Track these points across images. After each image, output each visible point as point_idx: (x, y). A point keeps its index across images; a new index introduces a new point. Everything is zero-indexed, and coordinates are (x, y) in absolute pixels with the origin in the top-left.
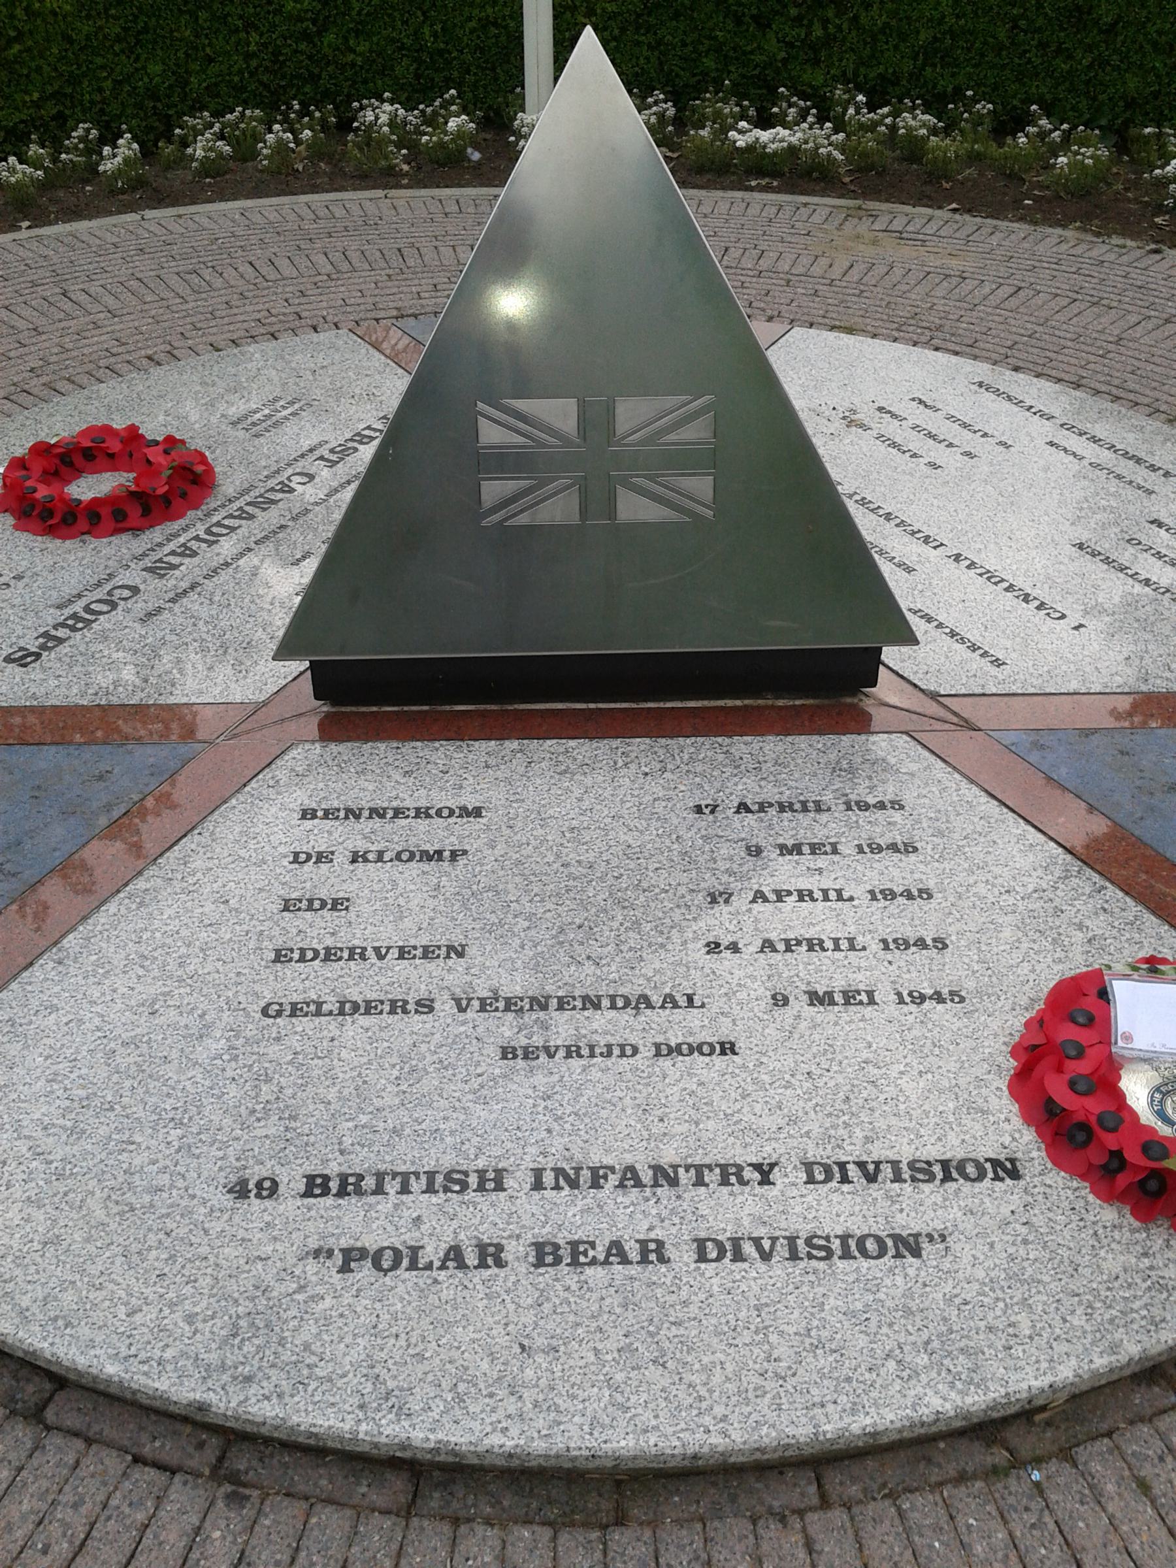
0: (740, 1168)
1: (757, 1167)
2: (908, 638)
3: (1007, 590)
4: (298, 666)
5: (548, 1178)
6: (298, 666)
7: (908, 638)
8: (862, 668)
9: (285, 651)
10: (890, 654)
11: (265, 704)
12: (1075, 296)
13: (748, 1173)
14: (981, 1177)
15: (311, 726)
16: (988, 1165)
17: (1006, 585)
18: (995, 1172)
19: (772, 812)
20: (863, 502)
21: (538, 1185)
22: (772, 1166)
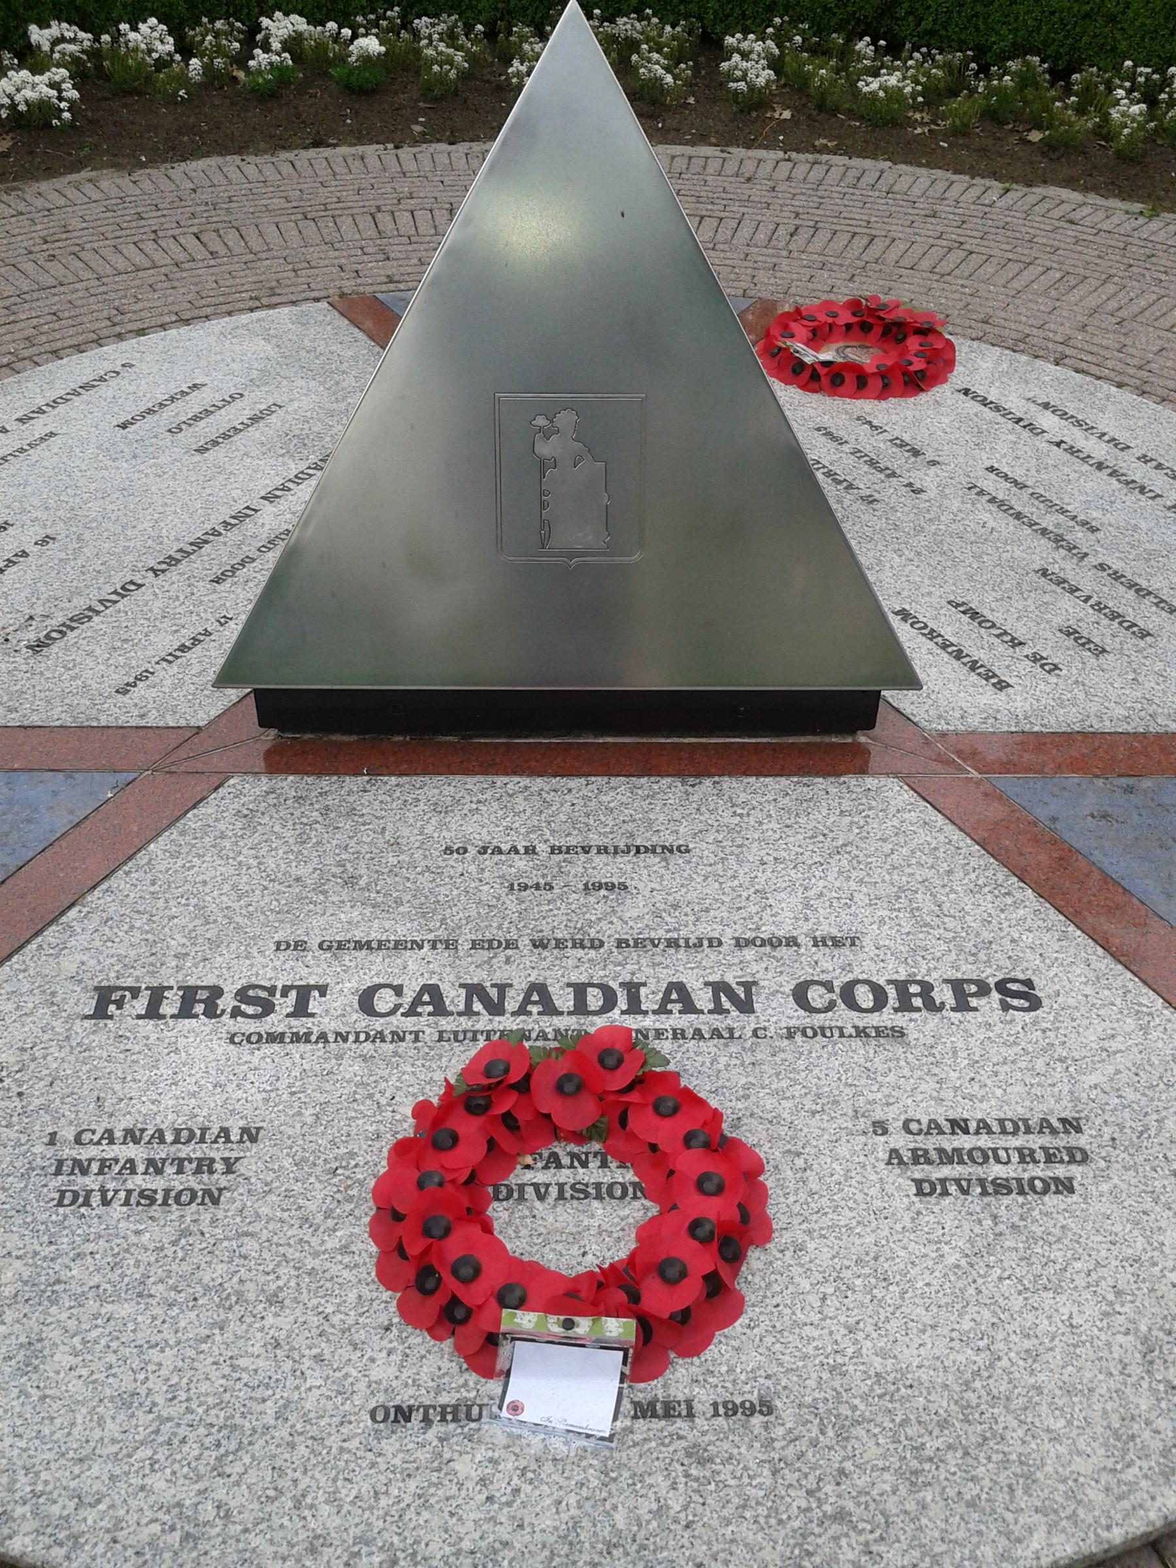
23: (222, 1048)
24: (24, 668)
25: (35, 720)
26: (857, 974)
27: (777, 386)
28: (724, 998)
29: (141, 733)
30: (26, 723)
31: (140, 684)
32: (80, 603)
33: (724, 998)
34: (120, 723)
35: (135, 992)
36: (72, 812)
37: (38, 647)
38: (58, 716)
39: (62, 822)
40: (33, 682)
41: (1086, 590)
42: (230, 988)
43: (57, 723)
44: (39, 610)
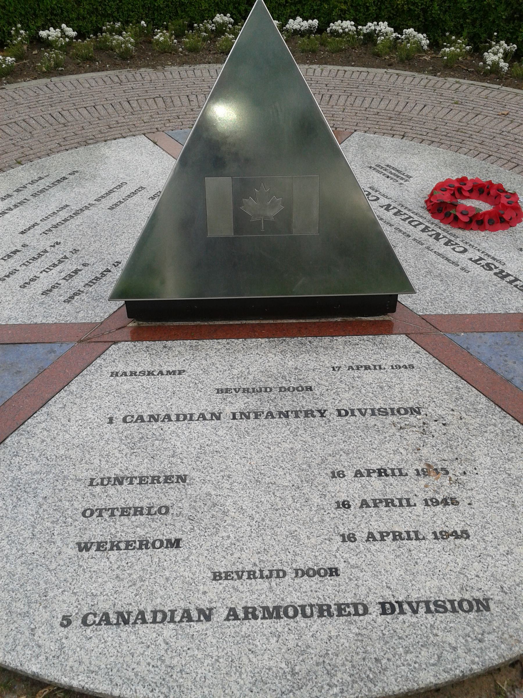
0: (313, 412)
1: (319, 411)
2: (409, 289)
3: (423, 231)
4: (121, 303)
5: (238, 416)
6: (121, 303)
7: (409, 289)
8: (389, 304)
9: (115, 296)
10: (403, 298)
11: (102, 323)
12: (460, 145)
13: (316, 413)
14: (471, 610)
15: (126, 332)
16: (474, 603)
17: (423, 227)
18: (478, 606)
19: (382, 506)
20: (381, 219)
21: (234, 418)
22: (325, 411)
23: (508, 265)
24: (432, 405)
25: (455, 378)
26: (155, 538)
27: (301, 69)
28: (120, 619)
29: (426, 347)
30: (459, 379)
31: (401, 364)
32: (372, 421)
33: (120, 619)
34: (428, 355)
35: (516, 286)
36: (481, 337)
37: (415, 411)
38: (445, 373)
39: (488, 337)
40: (437, 395)
41: (157, 368)
42: (492, 273)
43: (449, 371)
44: (393, 430)
